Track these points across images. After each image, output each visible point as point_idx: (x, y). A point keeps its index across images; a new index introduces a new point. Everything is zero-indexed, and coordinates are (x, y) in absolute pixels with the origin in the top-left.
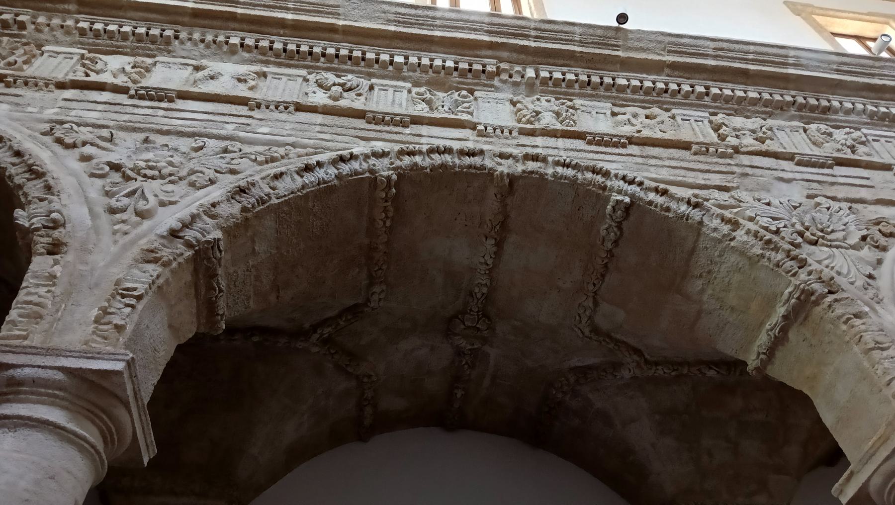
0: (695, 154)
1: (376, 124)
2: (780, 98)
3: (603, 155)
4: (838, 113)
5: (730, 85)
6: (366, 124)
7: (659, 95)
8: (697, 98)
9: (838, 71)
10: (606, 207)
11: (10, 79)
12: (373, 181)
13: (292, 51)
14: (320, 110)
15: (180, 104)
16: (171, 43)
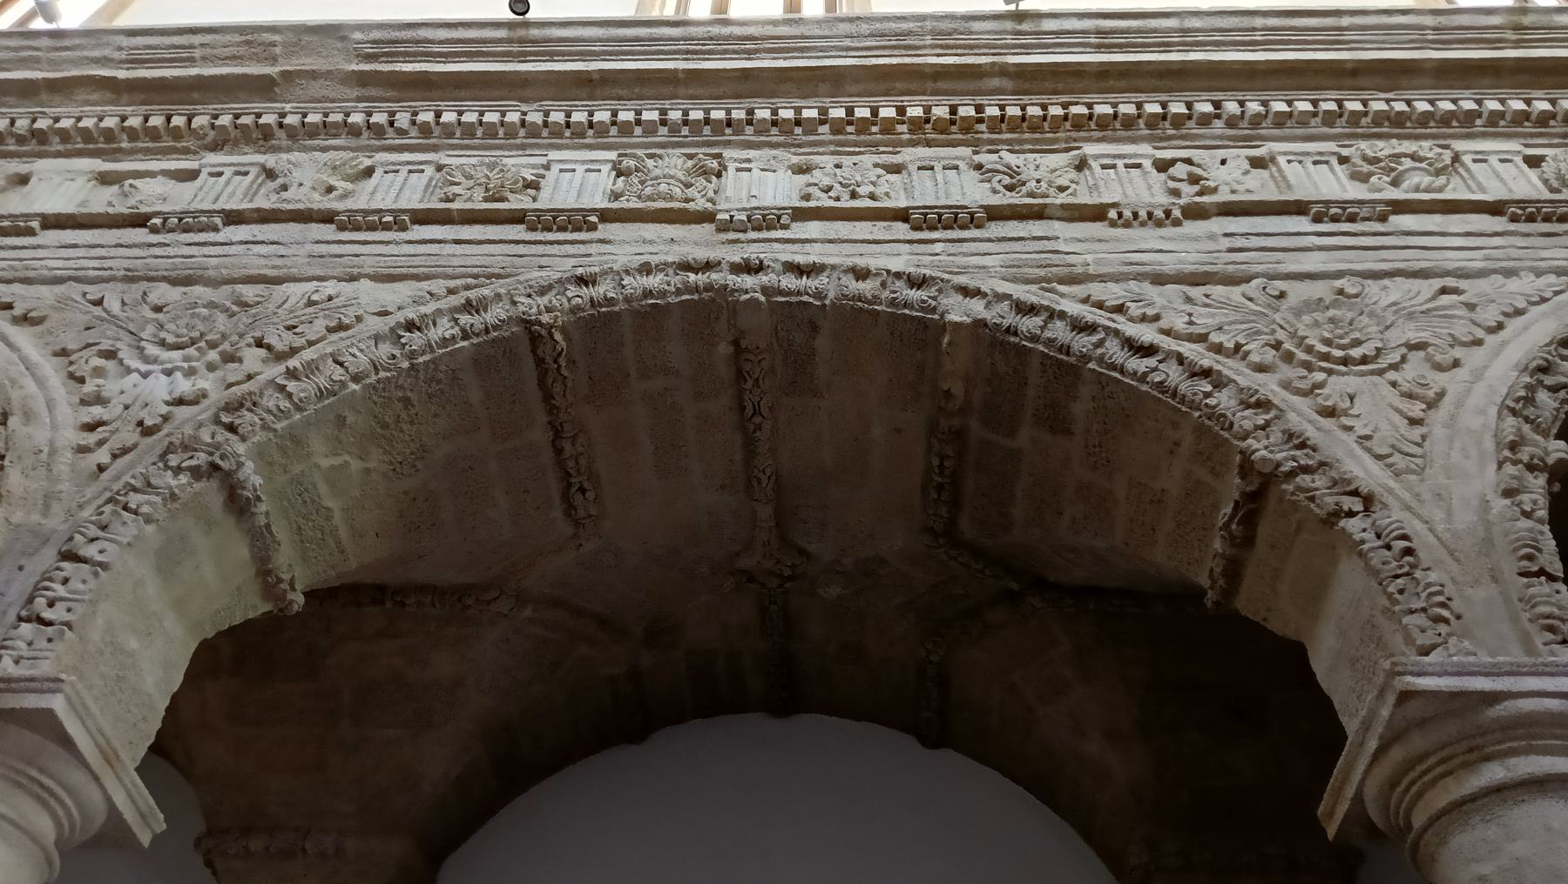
1: (945, 228)
2: (1452, 107)
3: (1045, 242)
4: (1210, 124)
5: (1334, 95)
6: (912, 232)
7: (1054, 130)
8: (1373, 122)
9: (1099, 48)
10: (941, 344)
11: (157, 221)
12: (532, 333)
13: (581, 123)
14: (314, 216)
15: (605, 230)
16: (47, 140)
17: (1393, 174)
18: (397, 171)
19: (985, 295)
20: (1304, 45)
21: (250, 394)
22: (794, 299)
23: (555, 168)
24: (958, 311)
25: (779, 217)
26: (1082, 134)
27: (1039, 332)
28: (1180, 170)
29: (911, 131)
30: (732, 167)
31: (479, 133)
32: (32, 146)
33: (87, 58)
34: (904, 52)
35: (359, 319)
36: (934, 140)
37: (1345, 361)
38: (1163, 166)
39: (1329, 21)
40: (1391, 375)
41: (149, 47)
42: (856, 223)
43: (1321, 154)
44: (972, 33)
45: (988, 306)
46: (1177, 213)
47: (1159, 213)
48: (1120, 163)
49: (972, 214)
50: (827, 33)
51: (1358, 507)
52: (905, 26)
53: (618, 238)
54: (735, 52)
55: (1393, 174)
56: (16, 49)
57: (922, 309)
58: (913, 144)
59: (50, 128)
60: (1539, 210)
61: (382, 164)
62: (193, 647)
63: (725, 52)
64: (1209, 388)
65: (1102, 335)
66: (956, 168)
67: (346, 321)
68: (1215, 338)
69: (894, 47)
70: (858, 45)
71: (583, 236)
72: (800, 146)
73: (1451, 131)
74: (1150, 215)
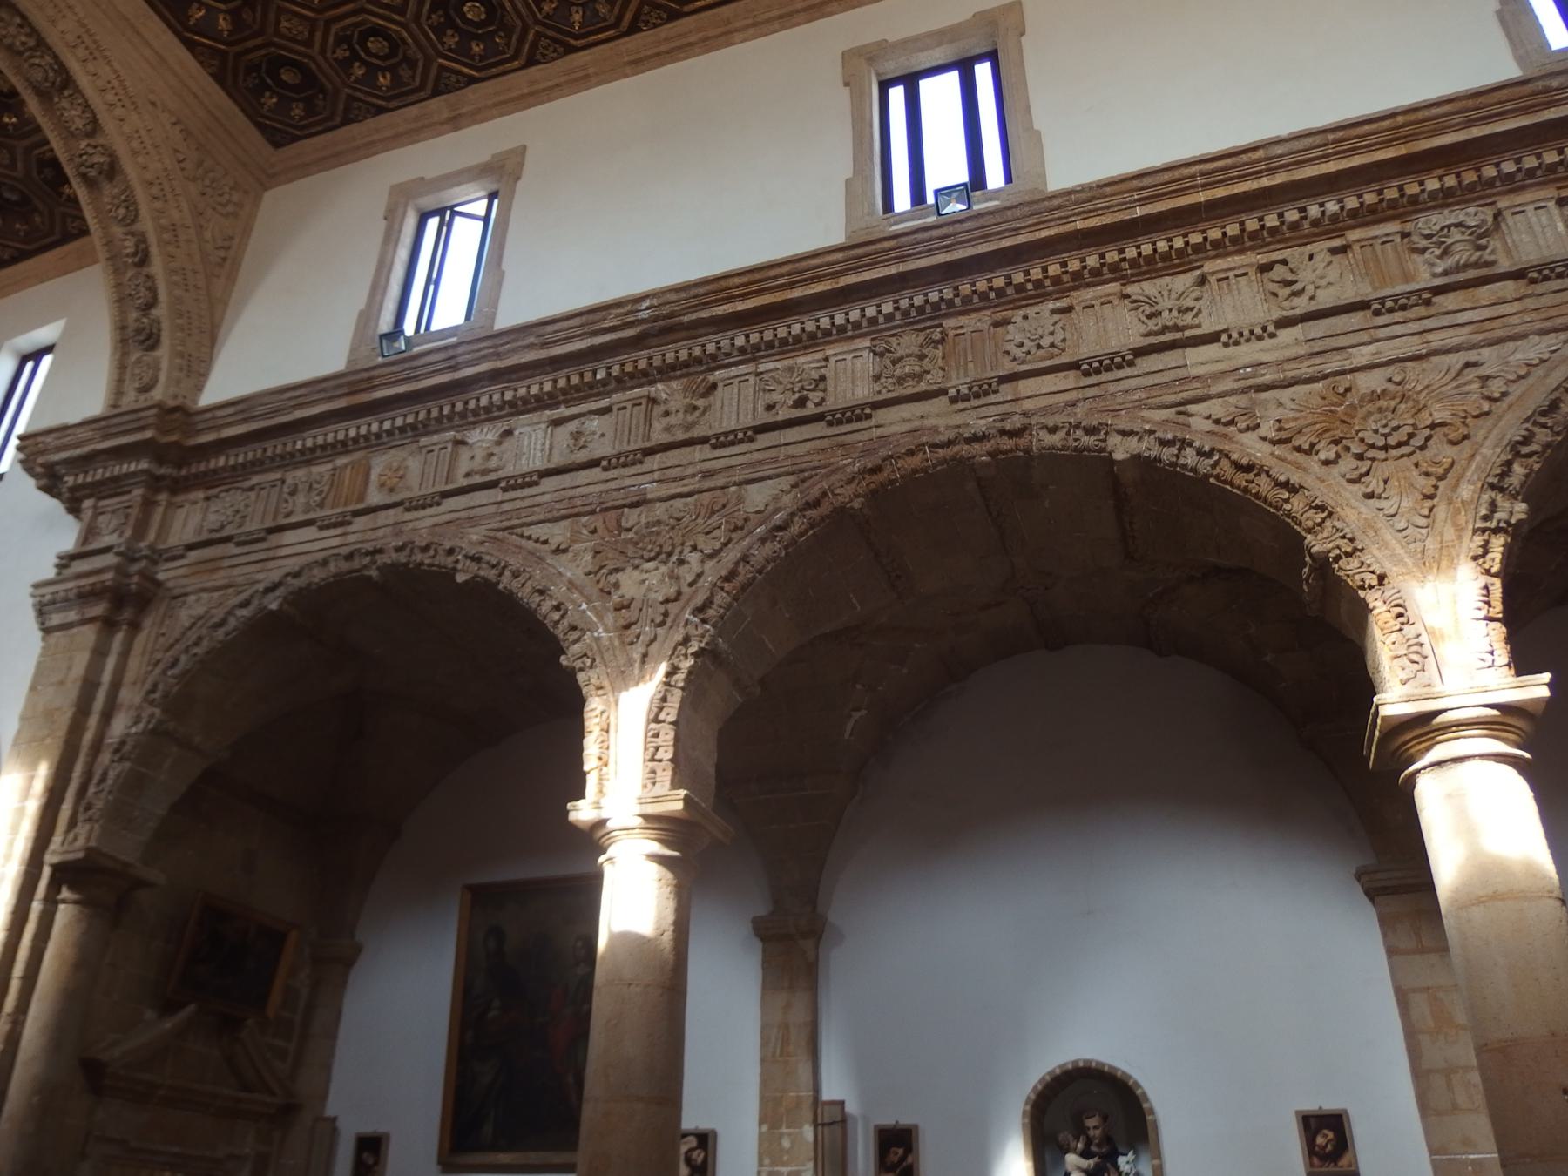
17: (1443, 246)
18: (731, 384)
19: (1137, 433)
20: (1368, 149)
22: (1010, 455)
23: (833, 360)
24: (1121, 449)
25: (990, 385)
26: (1200, 256)
27: (1175, 459)
28: (1279, 272)
30: (951, 333)
33: (520, 347)
34: (1058, 222)
35: (746, 520)
36: (1092, 282)
37: (1385, 448)
38: (1264, 268)
39: (1386, 123)
40: (1418, 456)
41: (556, 332)
42: (1044, 377)
43: (1387, 235)
44: (1106, 196)
45: (1140, 439)
46: (1271, 328)
47: (1258, 331)
48: (1231, 274)
49: (1123, 357)
50: (999, 220)
51: (1375, 582)
52: (1056, 202)
53: (887, 422)
54: (937, 249)
55: (1443, 246)
56: (478, 351)
57: (1095, 451)
58: (1075, 288)
59: (515, 396)
60: (1552, 270)
61: (723, 380)
63: (930, 250)
64: (1286, 495)
65: (1216, 458)
66: (1111, 302)
67: (740, 524)
68: (1297, 442)
70: (1023, 225)
71: (864, 424)
72: (995, 306)
73: (1495, 190)
74: (1252, 332)
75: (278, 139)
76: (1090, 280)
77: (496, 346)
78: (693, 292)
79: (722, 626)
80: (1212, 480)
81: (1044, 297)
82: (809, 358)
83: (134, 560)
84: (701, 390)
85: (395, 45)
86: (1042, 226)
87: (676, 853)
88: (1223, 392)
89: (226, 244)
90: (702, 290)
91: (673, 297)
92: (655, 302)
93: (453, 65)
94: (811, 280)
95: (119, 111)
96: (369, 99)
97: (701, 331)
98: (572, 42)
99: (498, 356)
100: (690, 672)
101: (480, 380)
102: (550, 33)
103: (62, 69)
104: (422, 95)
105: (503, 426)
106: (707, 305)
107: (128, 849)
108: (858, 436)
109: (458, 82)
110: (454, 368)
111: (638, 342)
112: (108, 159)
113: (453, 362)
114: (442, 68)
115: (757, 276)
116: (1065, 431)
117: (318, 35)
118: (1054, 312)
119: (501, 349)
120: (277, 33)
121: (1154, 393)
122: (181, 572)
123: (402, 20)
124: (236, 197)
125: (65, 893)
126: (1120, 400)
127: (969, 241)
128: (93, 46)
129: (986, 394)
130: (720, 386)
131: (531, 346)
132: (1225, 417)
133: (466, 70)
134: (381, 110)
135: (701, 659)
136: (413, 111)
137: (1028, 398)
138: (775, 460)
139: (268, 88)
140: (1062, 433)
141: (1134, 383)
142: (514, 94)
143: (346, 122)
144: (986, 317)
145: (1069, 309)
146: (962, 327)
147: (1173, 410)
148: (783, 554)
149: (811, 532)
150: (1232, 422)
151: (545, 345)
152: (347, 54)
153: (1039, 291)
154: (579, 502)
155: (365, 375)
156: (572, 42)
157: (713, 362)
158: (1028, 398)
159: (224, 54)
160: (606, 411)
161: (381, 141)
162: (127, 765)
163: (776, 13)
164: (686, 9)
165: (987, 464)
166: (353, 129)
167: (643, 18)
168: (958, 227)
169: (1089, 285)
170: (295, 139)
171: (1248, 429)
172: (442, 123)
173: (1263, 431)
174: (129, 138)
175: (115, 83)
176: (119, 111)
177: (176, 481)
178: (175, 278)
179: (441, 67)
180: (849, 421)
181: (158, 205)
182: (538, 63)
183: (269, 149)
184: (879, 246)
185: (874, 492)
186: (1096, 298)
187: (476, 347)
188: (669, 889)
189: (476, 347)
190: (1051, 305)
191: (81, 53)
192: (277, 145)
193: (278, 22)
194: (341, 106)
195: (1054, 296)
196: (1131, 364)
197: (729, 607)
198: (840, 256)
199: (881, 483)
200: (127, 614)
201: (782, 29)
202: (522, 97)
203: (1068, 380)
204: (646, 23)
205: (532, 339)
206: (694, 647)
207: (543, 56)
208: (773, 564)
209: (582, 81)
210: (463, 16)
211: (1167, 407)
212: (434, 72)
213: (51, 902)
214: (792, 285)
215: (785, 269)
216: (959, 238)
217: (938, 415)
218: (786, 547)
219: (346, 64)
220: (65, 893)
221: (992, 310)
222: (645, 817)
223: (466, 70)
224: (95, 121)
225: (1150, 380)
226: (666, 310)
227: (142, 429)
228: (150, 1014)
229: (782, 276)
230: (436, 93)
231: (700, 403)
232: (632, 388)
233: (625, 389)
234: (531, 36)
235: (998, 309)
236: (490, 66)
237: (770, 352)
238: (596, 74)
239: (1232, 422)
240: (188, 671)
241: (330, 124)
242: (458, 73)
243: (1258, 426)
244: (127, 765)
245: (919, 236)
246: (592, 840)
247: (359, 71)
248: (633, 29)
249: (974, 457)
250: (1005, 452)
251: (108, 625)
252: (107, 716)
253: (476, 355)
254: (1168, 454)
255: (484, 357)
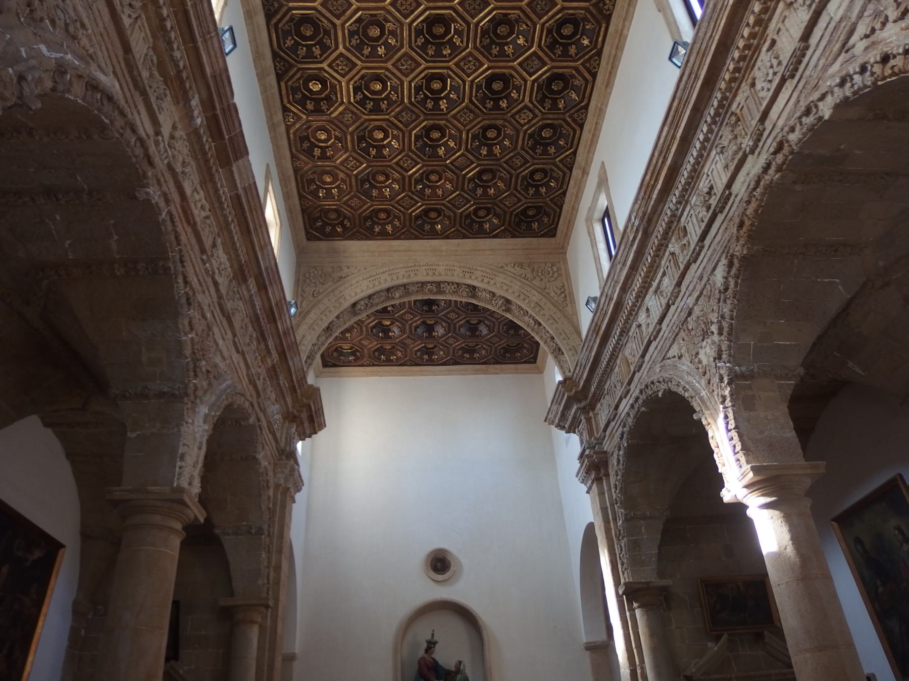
0: (202, 259)
19: (827, 93)
21: (812, 102)
22: (787, 162)
23: (710, 173)
24: (826, 110)
25: (759, 130)
29: (760, 26)
30: (738, 111)
31: (696, 167)
32: (640, 300)
34: (722, 12)
50: (700, 42)
54: (693, 83)
58: (766, 28)
61: (685, 222)
62: (784, 408)
63: (692, 87)
66: (785, 17)
69: (716, 23)
72: (744, 77)
75: (552, 233)
76: (767, 16)
77: (613, 280)
78: (640, 197)
79: (733, 359)
80: (880, 83)
81: (758, 49)
82: (703, 181)
83: (594, 447)
84: (682, 234)
85: (543, 171)
86: (718, 23)
87: (774, 498)
88: (859, 13)
89: (562, 290)
90: (642, 194)
91: (637, 206)
92: (634, 214)
93: (562, 157)
94: (669, 149)
95: (492, 282)
96: (556, 194)
97: (660, 209)
98: (582, 104)
99: (617, 282)
100: (731, 395)
101: (622, 296)
102: (572, 111)
103: (469, 286)
104: (568, 175)
105: (644, 309)
106: (650, 197)
107: (649, 575)
108: (733, 209)
109: (571, 158)
110: (611, 299)
111: (647, 235)
112: (503, 300)
113: (609, 297)
114: (561, 161)
115: (651, 168)
116: (798, 125)
117: (518, 195)
118: (768, 50)
119: (615, 279)
120: (509, 208)
121: (827, 54)
122: (608, 443)
123: (530, 164)
124: (555, 269)
125: (635, 605)
126: (815, 76)
127: (700, 65)
128: (469, 270)
129: (761, 135)
130: (686, 225)
131: (621, 270)
132: (867, 30)
133: (567, 153)
134: (564, 193)
135: (734, 384)
136: (572, 182)
137: (778, 119)
138: (715, 250)
139: (531, 222)
140: (798, 127)
141: (815, 58)
142: (589, 143)
143: (561, 208)
144: (745, 87)
145: (774, 42)
146: (739, 104)
147: (843, 54)
148: (736, 302)
149: (739, 281)
150: (873, 30)
151: (624, 264)
152: (534, 189)
153: (752, 49)
154: (674, 328)
155: (594, 324)
156: (582, 104)
157: (675, 218)
158: (778, 119)
159: (505, 229)
160: (664, 274)
161: (575, 203)
162: (625, 539)
163: (626, 6)
164: (599, 47)
165: (782, 177)
166: (565, 207)
167: (591, 68)
168: (690, 65)
169: (770, 19)
170: (556, 228)
171: (884, 24)
172: (583, 177)
173: (891, 18)
174: (502, 287)
175: (484, 274)
176: (492, 282)
177: (590, 405)
178: (550, 322)
179: (560, 161)
180: (726, 203)
181: (527, 301)
182: (583, 124)
183: (553, 239)
184: (674, 108)
185: (749, 237)
186: (777, 23)
187: (608, 285)
188: (780, 520)
189: (608, 285)
190: (765, 48)
191: (467, 275)
192: (554, 236)
193: (505, 205)
194: (553, 206)
195: (762, 42)
196: (807, 48)
197: (729, 347)
198: (666, 129)
199: (748, 230)
200: (602, 471)
201: (634, 8)
202: (592, 141)
203: (789, 85)
204: (595, 68)
205: (619, 267)
206: (726, 380)
207: (582, 119)
208: (735, 311)
209: (601, 112)
210: (546, 138)
211: (839, 55)
212: (561, 165)
213: (632, 610)
214: (665, 159)
215: (656, 154)
216: (696, 68)
217: (753, 167)
218: (734, 297)
219: (537, 193)
220: (635, 605)
221: (744, 81)
222: (746, 487)
223: (567, 153)
224: (493, 293)
225: (821, 47)
226: (640, 214)
227: (564, 395)
228: (710, 644)
229: (658, 159)
230: (571, 170)
231: (685, 242)
232: (664, 254)
233: (662, 257)
234: (569, 120)
235: (746, 78)
236: (573, 144)
237: (689, 193)
238: (602, 104)
239: (873, 30)
240: (621, 488)
241: (557, 214)
242: (567, 156)
243: (887, 18)
244: (625, 539)
245: (682, 86)
246: (739, 508)
247: (543, 190)
248: (594, 76)
249: (772, 180)
250: (784, 163)
251: (598, 480)
252: (615, 519)
253: (611, 288)
254: (848, 91)
255: (614, 286)
